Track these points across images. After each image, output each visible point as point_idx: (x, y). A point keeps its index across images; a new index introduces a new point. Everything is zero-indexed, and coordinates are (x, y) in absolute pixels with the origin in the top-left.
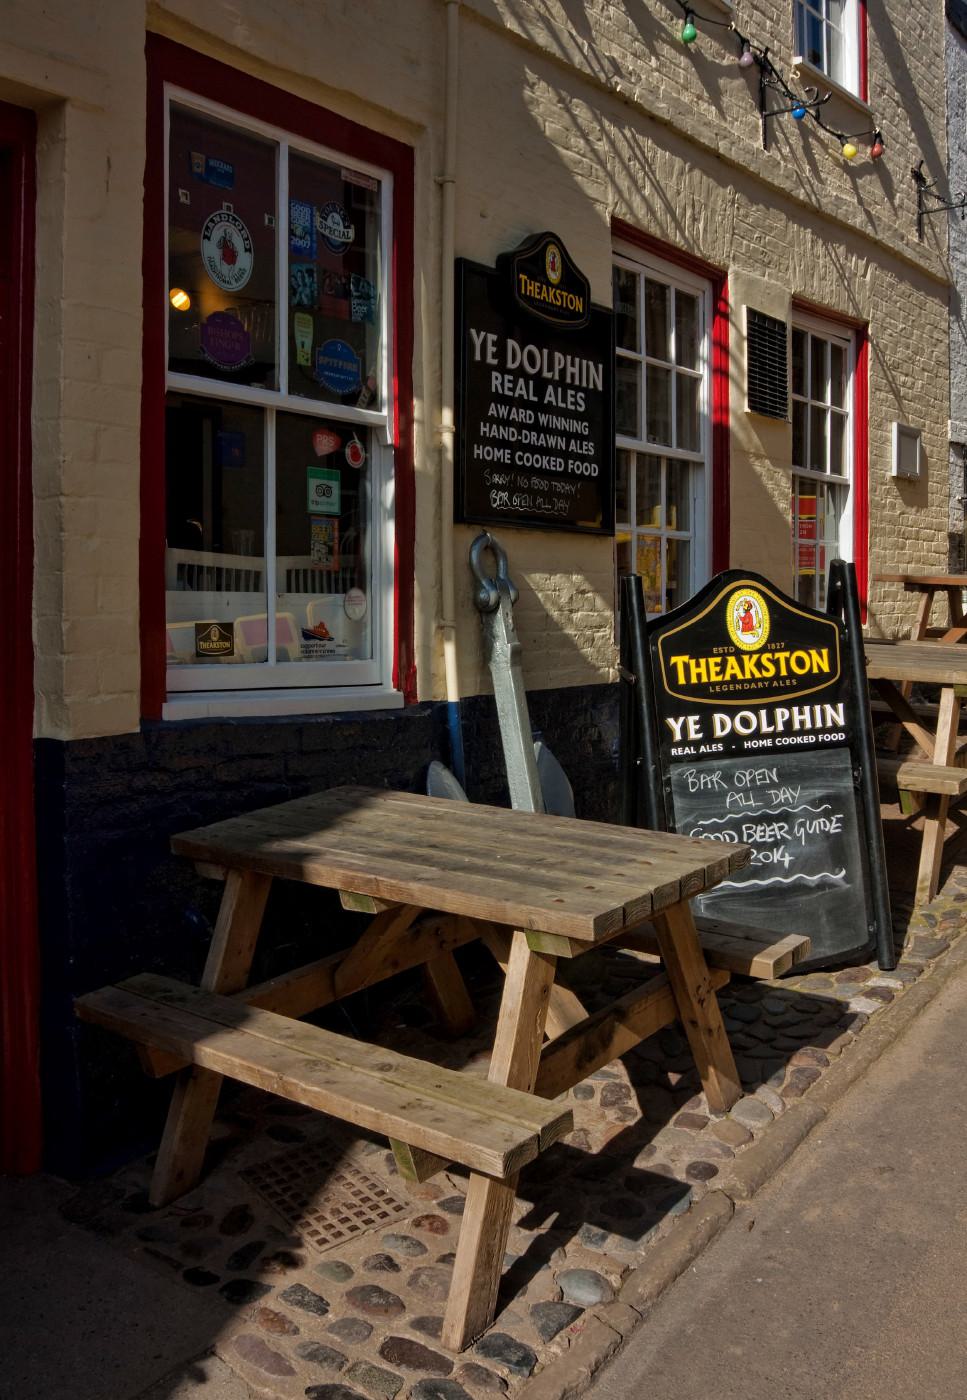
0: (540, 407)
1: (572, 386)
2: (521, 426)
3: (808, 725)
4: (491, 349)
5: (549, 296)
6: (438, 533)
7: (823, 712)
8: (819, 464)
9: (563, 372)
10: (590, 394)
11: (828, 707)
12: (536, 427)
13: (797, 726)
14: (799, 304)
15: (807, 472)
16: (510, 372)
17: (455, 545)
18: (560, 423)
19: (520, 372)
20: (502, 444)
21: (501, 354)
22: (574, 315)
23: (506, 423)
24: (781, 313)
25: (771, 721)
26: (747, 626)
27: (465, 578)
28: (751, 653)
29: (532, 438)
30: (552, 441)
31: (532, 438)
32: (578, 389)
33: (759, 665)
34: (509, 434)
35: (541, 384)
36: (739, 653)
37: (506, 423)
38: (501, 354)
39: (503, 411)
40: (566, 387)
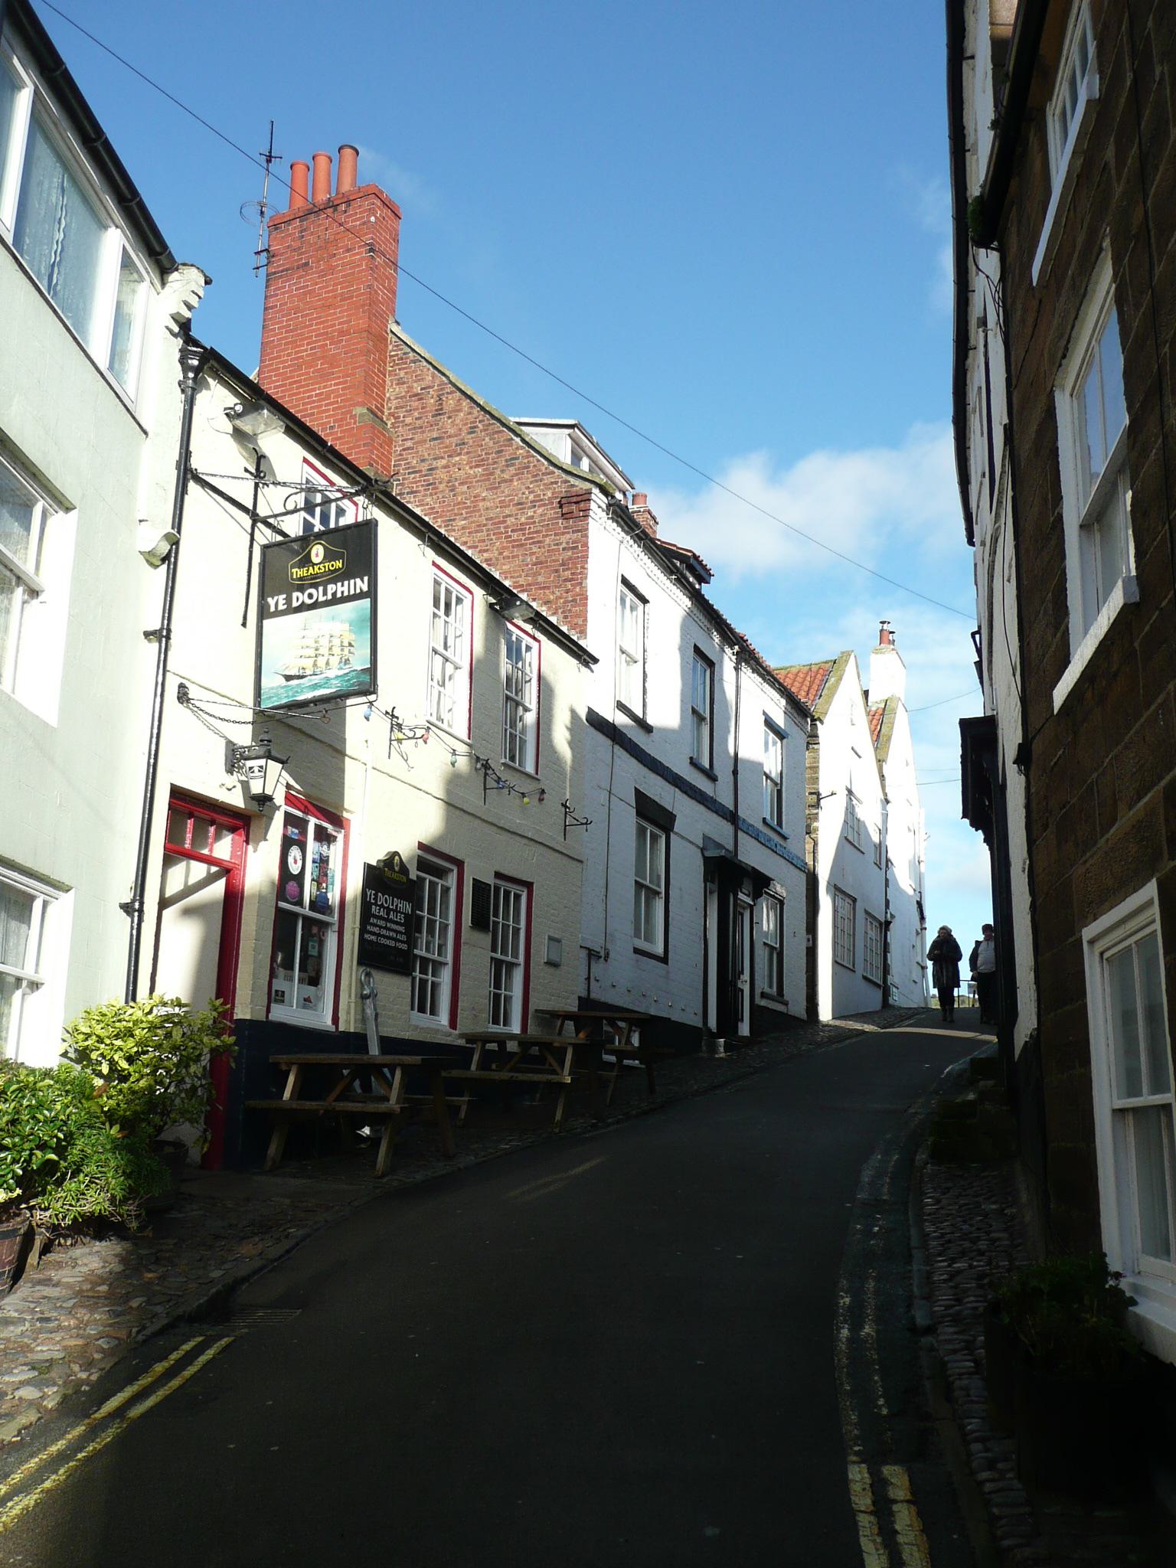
0: (388, 920)
1: (399, 912)
2: (381, 927)
3: (346, 594)
4: (373, 897)
5: (395, 876)
6: (351, 967)
7: (355, 583)
8: (504, 952)
9: (397, 906)
10: (406, 915)
11: (358, 580)
12: (386, 928)
13: (339, 595)
14: (498, 875)
15: (498, 956)
16: (378, 905)
17: (357, 970)
18: (394, 927)
19: (382, 906)
20: (373, 934)
21: (376, 899)
22: (404, 883)
23: (375, 925)
24: (490, 880)
25: (325, 593)
26: (317, 555)
27: (359, 985)
28: (317, 564)
29: (384, 932)
30: (391, 934)
31: (384, 932)
32: (402, 913)
33: (319, 569)
34: (376, 930)
35: (388, 910)
36: (314, 565)
37: (375, 925)
38: (376, 899)
39: (375, 921)
40: (397, 912)
